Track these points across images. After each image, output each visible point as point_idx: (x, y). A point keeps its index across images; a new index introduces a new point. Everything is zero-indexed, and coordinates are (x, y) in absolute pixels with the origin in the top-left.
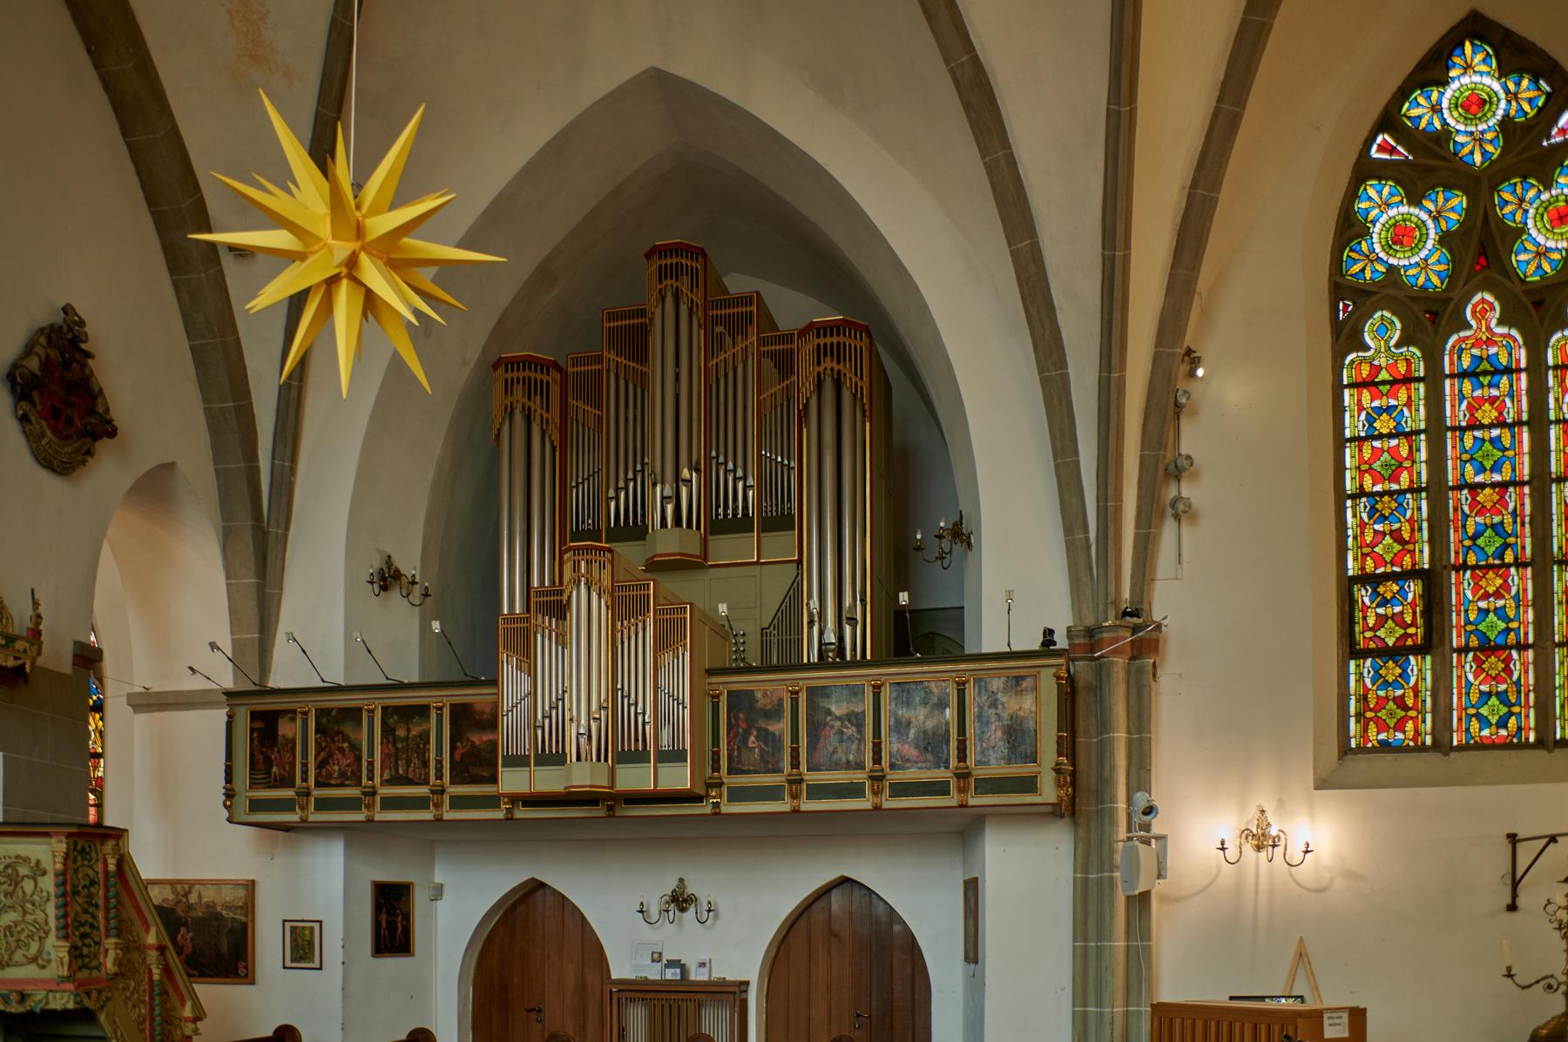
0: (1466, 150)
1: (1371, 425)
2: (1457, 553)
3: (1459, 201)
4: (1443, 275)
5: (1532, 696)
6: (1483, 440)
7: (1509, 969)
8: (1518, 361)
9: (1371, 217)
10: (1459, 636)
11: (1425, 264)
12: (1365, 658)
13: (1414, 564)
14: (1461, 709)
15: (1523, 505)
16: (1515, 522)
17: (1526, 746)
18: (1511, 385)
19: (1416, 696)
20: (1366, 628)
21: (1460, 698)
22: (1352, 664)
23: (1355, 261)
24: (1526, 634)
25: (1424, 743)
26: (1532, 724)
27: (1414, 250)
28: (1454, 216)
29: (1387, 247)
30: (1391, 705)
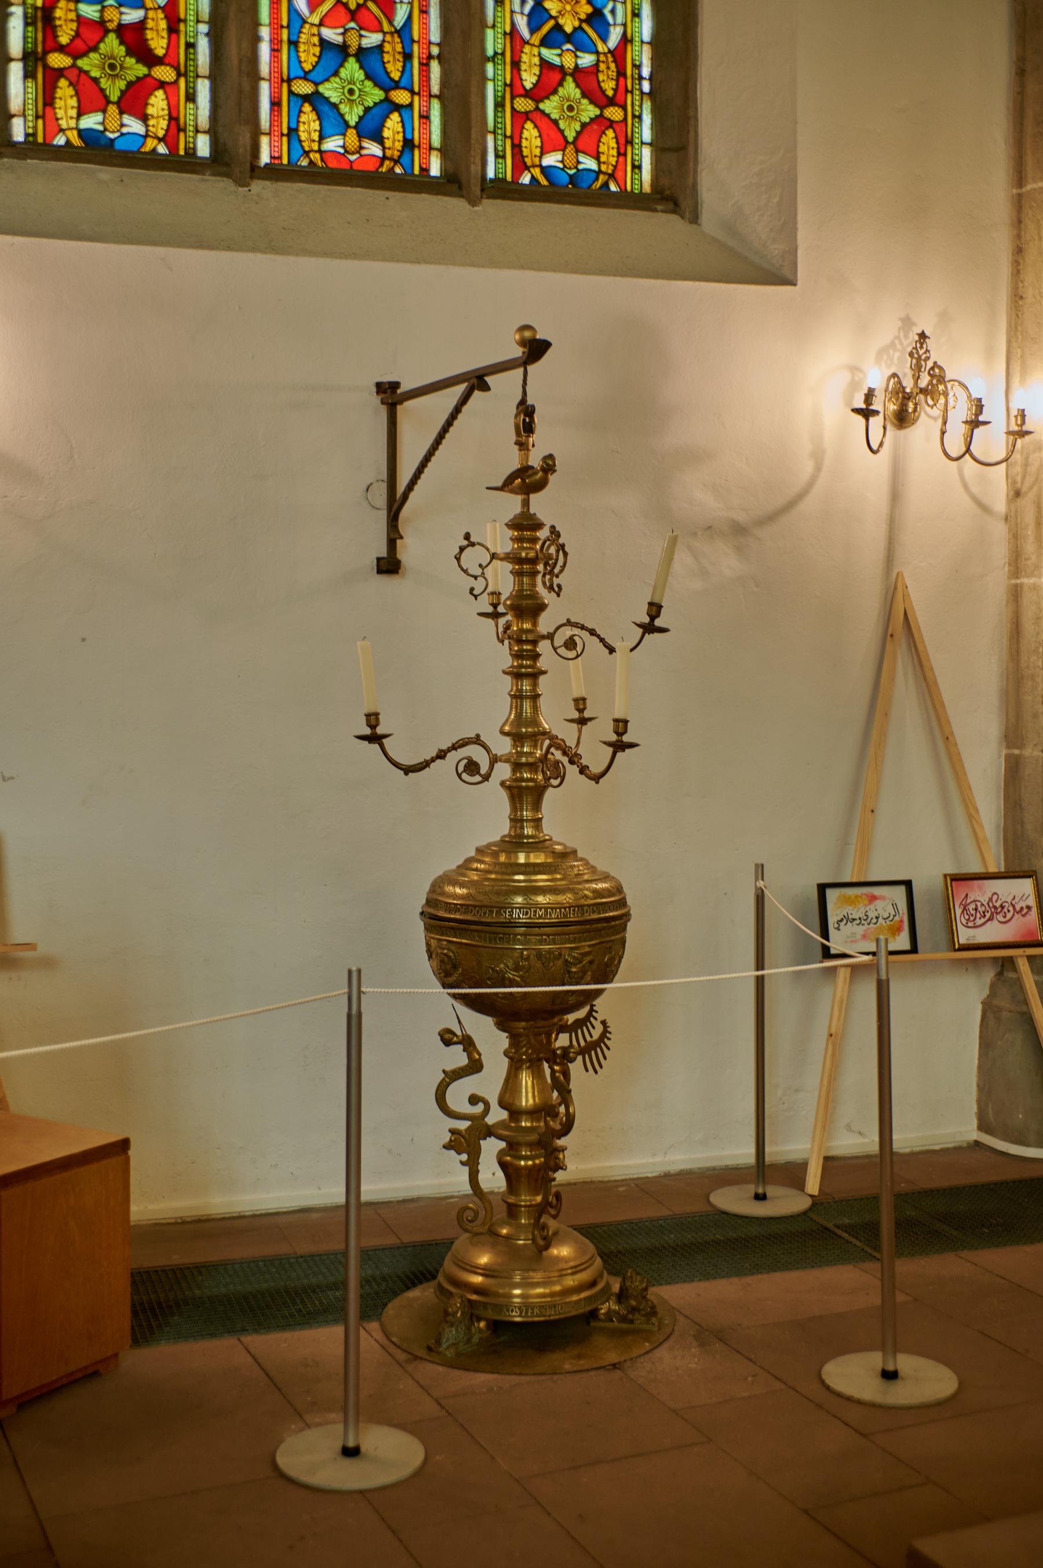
5: (435, 68)
7: (372, 719)
17: (422, 184)
19: (173, 29)
21: (275, 51)
25: (191, 152)
26: (436, 140)
30: (112, 44)
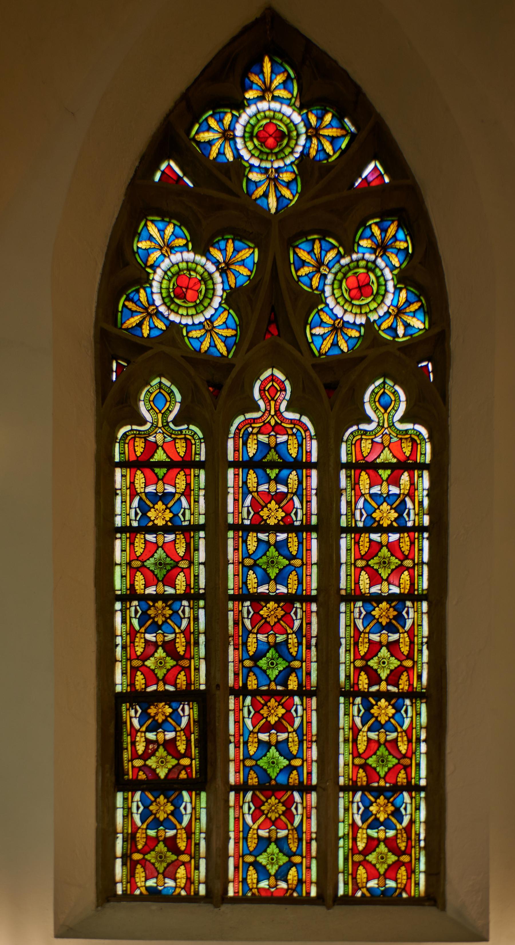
0: (260, 191)
1: (144, 514)
2: (236, 674)
3: (249, 255)
4: (231, 341)
5: (314, 844)
6: (268, 543)
8: (309, 453)
9: (152, 259)
10: (237, 771)
11: (210, 326)
12: (134, 792)
13: (189, 683)
14: (238, 856)
15: (309, 624)
16: (300, 644)
17: (308, 901)
18: (300, 482)
19: (189, 838)
20: (135, 756)
21: (237, 843)
22: (120, 796)
23: (133, 313)
24: (310, 774)
25: (197, 893)
26: (314, 878)
27: (199, 307)
28: (245, 271)
29: (168, 300)
30: (161, 847)
